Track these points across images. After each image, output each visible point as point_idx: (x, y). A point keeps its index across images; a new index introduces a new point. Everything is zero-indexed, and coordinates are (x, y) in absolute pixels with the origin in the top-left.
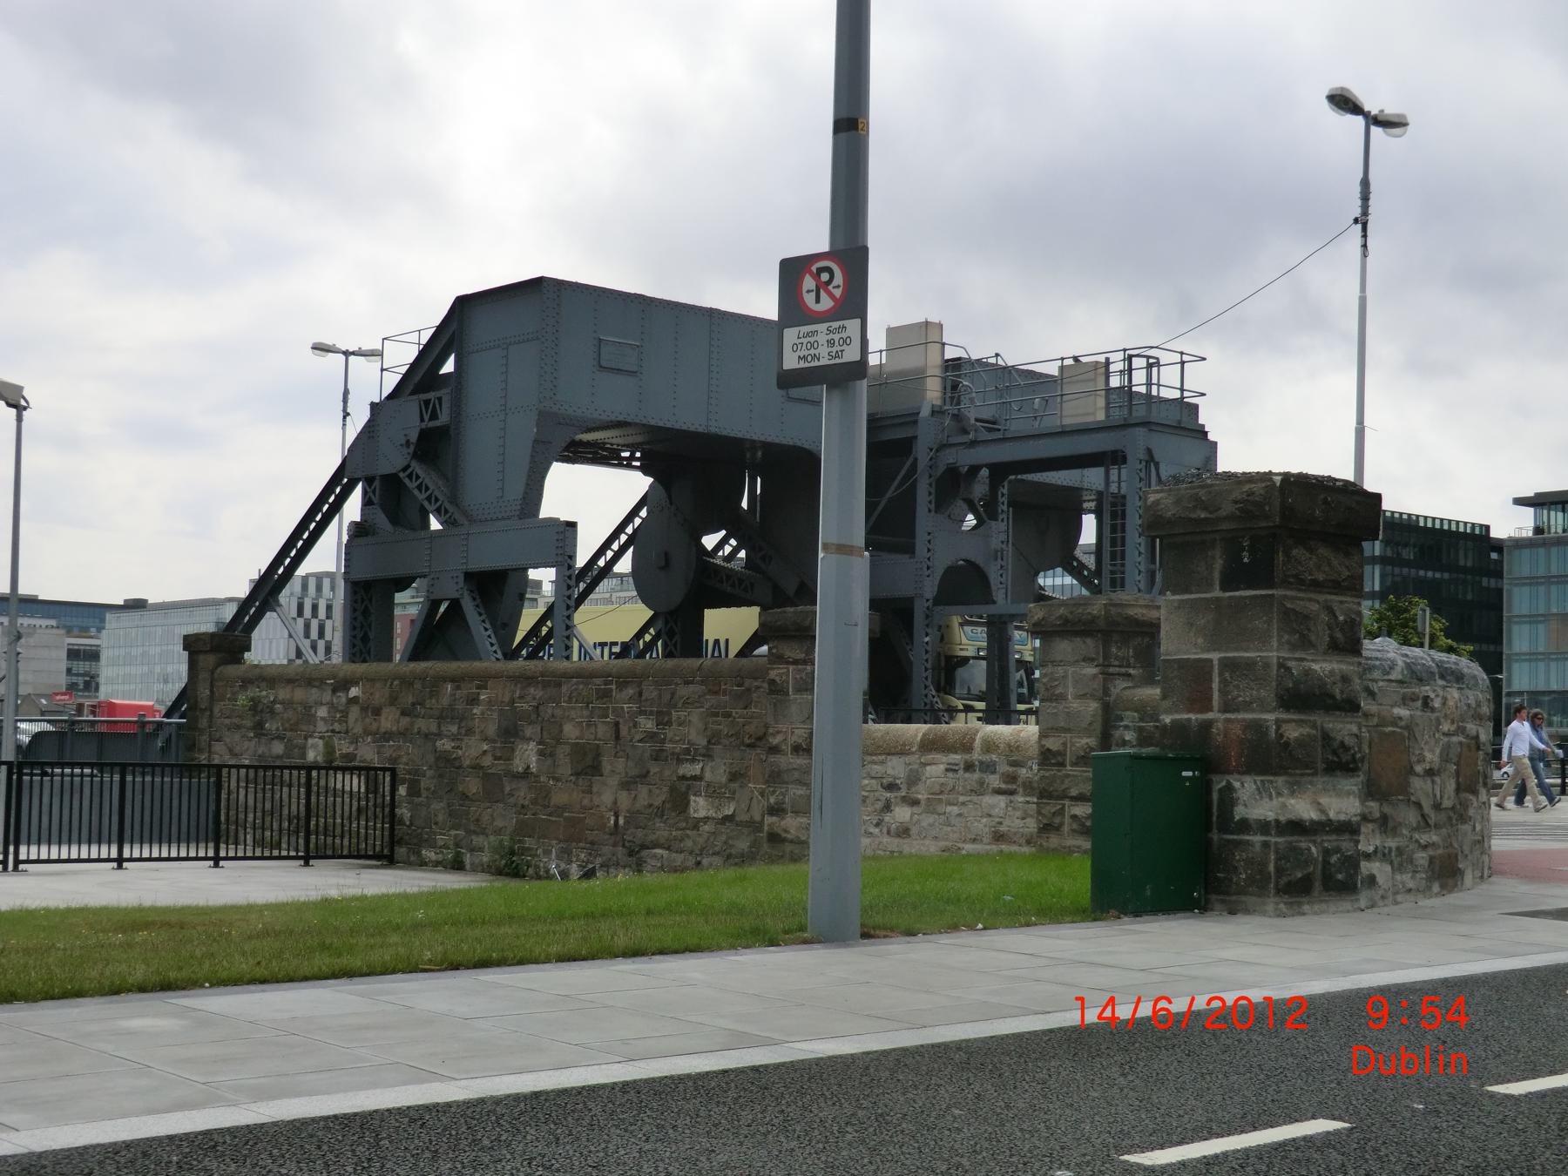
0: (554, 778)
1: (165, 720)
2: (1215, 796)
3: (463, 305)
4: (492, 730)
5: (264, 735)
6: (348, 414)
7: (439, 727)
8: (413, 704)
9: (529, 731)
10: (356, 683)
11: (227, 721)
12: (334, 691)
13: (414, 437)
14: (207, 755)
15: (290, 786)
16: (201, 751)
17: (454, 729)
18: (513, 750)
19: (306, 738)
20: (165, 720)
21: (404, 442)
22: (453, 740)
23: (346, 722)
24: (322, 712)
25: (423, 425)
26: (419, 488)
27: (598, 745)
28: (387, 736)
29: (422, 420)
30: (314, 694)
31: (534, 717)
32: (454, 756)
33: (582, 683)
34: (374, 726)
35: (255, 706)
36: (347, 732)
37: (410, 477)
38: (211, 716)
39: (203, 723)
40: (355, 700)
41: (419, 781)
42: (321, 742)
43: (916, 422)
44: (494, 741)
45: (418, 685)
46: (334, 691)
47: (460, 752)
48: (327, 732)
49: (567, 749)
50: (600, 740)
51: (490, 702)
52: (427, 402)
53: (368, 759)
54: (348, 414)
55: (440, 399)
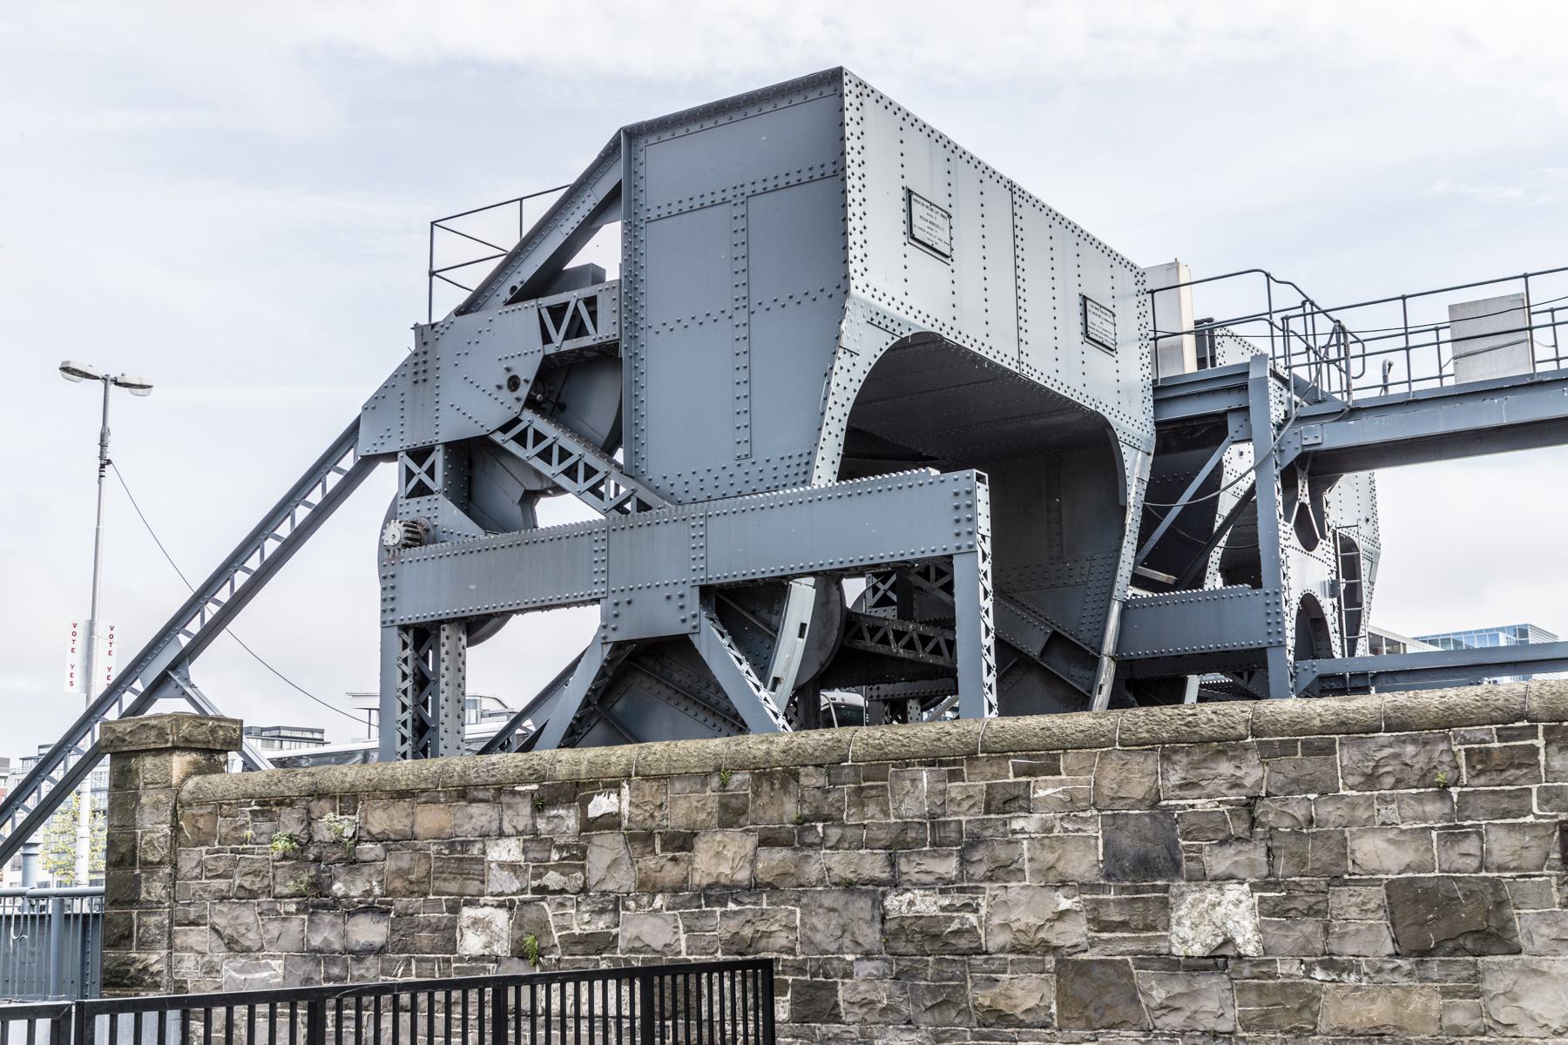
0: (1329, 965)
1: (986, 817)
2: (730, 958)
3: (633, 136)
4: (1084, 862)
5: (325, 906)
6: (109, 462)
7: (893, 864)
8: (801, 821)
9: (1220, 861)
10: (614, 786)
11: (222, 884)
12: (539, 806)
13: (527, 370)
14: (164, 953)
15: (674, 1018)
16: (145, 945)
17: (948, 867)
18: (1165, 905)
19: (454, 909)
20: (986, 817)
21: (504, 382)
22: (942, 892)
23: (583, 868)
24: (506, 851)
25: (550, 350)
26: (546, 455)
27: (1496, 884)
28: (718, 893)
29: (547, 339)
30: (480, 815)
31: (1237, 827)
32: (955, 926)
33: (1414, 741)
34: (672, 873)
35: (299, 853)
36: (584, 890)
37: (521, 439)
38: (174, 877)
39: (155, 889)
40: (610, 822)
41: (833, 988)
42: (501, 918)
43: (1244, 388)
44: (1093, 887)
45: (812, 779)
46: (539, 806)
47: (972, 918)
48: (523, 891)
49: (1377, 896)
50: (1500, 868)
51: (1070, 806)
52: (557, 312)
53: (658, 945)
54: (109, 462)
55: (591, 302)
